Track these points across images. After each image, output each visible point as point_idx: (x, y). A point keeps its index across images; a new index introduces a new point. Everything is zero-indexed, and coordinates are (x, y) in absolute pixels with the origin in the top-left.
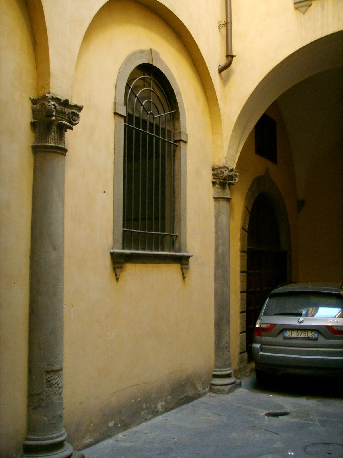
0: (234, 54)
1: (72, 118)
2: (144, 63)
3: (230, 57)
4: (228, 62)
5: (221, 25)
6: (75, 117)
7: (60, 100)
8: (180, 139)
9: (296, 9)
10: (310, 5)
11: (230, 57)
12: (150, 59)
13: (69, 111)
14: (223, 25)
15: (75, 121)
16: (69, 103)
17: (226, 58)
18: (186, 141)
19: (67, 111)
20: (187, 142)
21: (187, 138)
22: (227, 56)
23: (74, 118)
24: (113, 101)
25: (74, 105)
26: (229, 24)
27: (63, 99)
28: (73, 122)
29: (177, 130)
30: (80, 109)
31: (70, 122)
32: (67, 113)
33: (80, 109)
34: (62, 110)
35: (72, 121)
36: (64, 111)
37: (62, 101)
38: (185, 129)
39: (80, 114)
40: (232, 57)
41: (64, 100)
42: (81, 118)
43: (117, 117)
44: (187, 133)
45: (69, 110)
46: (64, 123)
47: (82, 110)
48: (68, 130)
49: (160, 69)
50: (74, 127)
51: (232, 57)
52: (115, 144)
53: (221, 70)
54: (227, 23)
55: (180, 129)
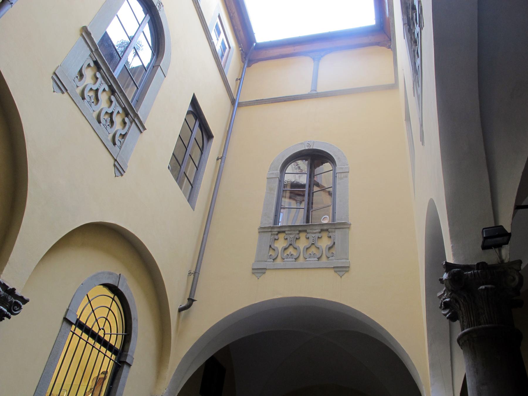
0: (195, 299)
1: (13, 308)
2: (110, 283)
3: (191, 301)
4: (188, 304)
5: (190, 273)
6: (16, 307)
7: (8, 287)
8: (125, 361)
9: (253, 273)
10: (264, 273)
11: (191, 301)
12: (117, 283)
13: (13, 300)
14: (192, 273)
15: (16, 311)
16: (15, 292)
17: (187, 301)
18: (131, 364)
19: (10, 299)
20: (131, 365)
21: (132, 361)
22: (189, 299)
23: (16, 308)
24: (67, 307)
25: (20, 295)
26: (197, 274)
27: (11, 287)
28: (13, 311)
29: (125, 352)
30: (25, 301)
31: (9, 310)
32: (9, 301)
33: (25, 301)
34: (5, 297)
35: (13, 311)
36: (7, 297)
37: (9, 289)
38: (133, 352)
39: (23, 306)
40: (193, 300)
41: (11, 288)
42: (22, 311)
43: (65, 323)
44: (134, 357)
45: (12, 298)
46: (2, 309)
47: (27, 303)
48: (5, 318)
49: (124, 293)
50: (12, 316)
51: (193, 300)
52: (54, 347)
53: (180, 310)
54: (195, 273)
55: (128, 352)
